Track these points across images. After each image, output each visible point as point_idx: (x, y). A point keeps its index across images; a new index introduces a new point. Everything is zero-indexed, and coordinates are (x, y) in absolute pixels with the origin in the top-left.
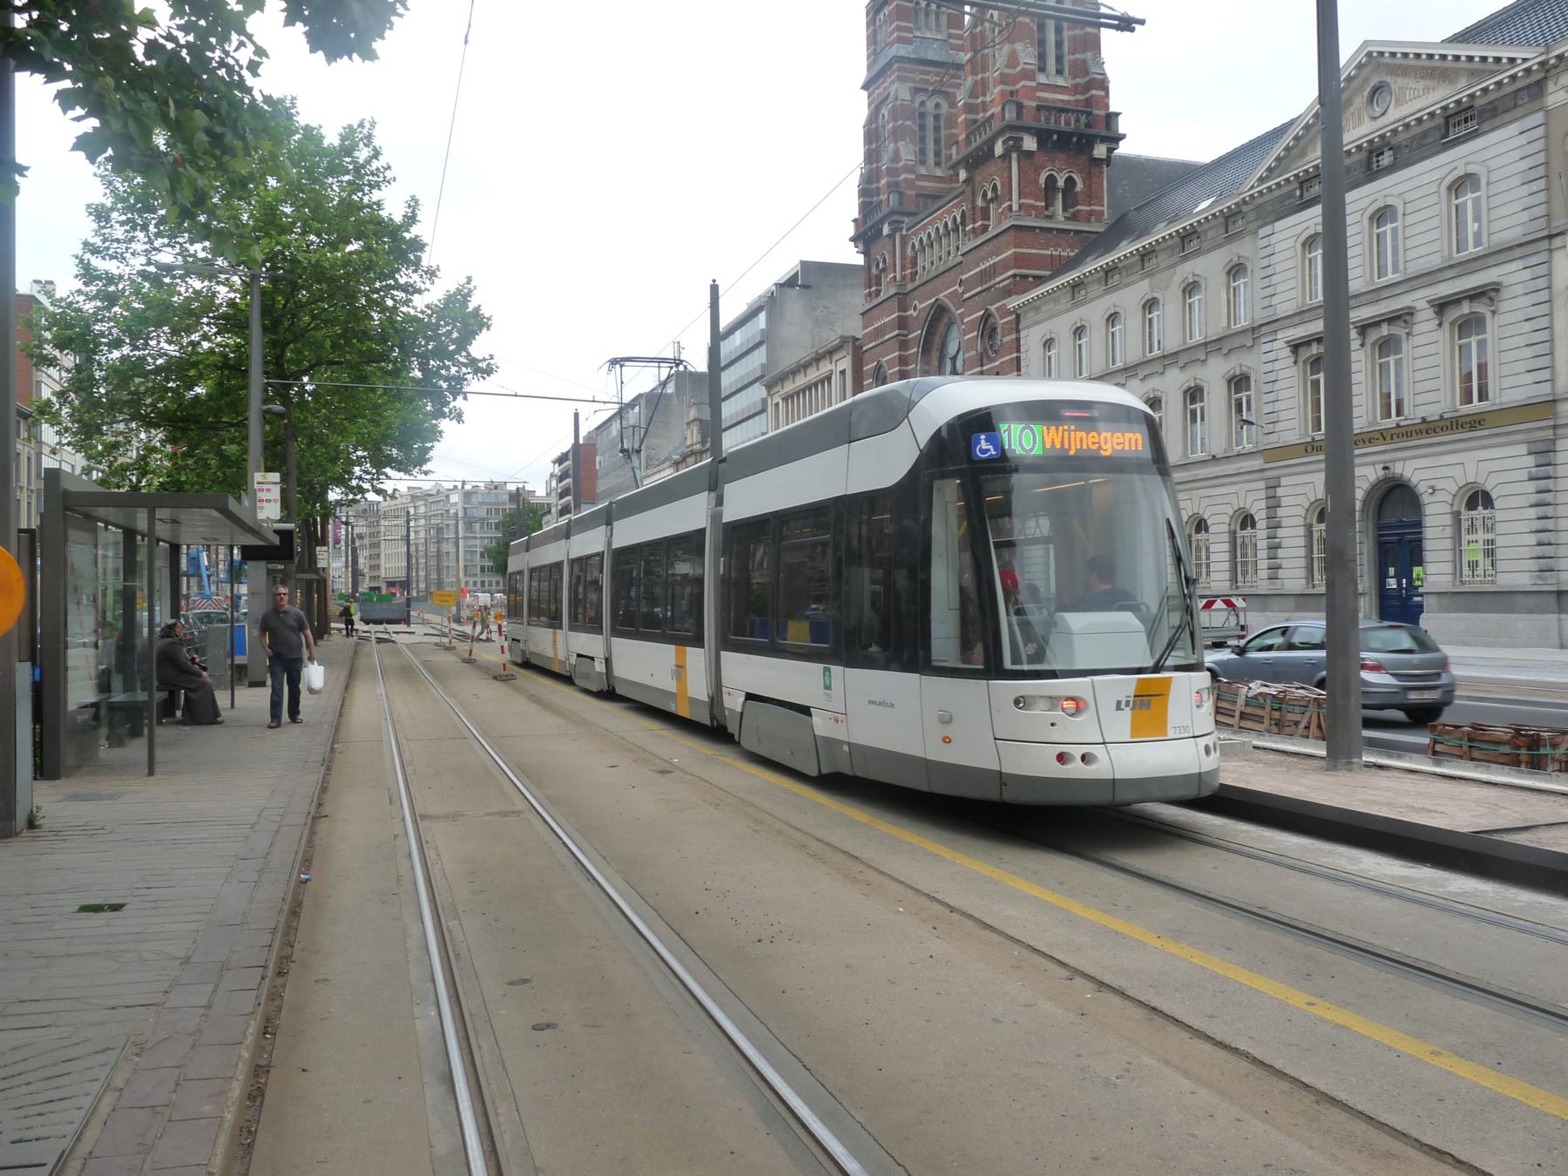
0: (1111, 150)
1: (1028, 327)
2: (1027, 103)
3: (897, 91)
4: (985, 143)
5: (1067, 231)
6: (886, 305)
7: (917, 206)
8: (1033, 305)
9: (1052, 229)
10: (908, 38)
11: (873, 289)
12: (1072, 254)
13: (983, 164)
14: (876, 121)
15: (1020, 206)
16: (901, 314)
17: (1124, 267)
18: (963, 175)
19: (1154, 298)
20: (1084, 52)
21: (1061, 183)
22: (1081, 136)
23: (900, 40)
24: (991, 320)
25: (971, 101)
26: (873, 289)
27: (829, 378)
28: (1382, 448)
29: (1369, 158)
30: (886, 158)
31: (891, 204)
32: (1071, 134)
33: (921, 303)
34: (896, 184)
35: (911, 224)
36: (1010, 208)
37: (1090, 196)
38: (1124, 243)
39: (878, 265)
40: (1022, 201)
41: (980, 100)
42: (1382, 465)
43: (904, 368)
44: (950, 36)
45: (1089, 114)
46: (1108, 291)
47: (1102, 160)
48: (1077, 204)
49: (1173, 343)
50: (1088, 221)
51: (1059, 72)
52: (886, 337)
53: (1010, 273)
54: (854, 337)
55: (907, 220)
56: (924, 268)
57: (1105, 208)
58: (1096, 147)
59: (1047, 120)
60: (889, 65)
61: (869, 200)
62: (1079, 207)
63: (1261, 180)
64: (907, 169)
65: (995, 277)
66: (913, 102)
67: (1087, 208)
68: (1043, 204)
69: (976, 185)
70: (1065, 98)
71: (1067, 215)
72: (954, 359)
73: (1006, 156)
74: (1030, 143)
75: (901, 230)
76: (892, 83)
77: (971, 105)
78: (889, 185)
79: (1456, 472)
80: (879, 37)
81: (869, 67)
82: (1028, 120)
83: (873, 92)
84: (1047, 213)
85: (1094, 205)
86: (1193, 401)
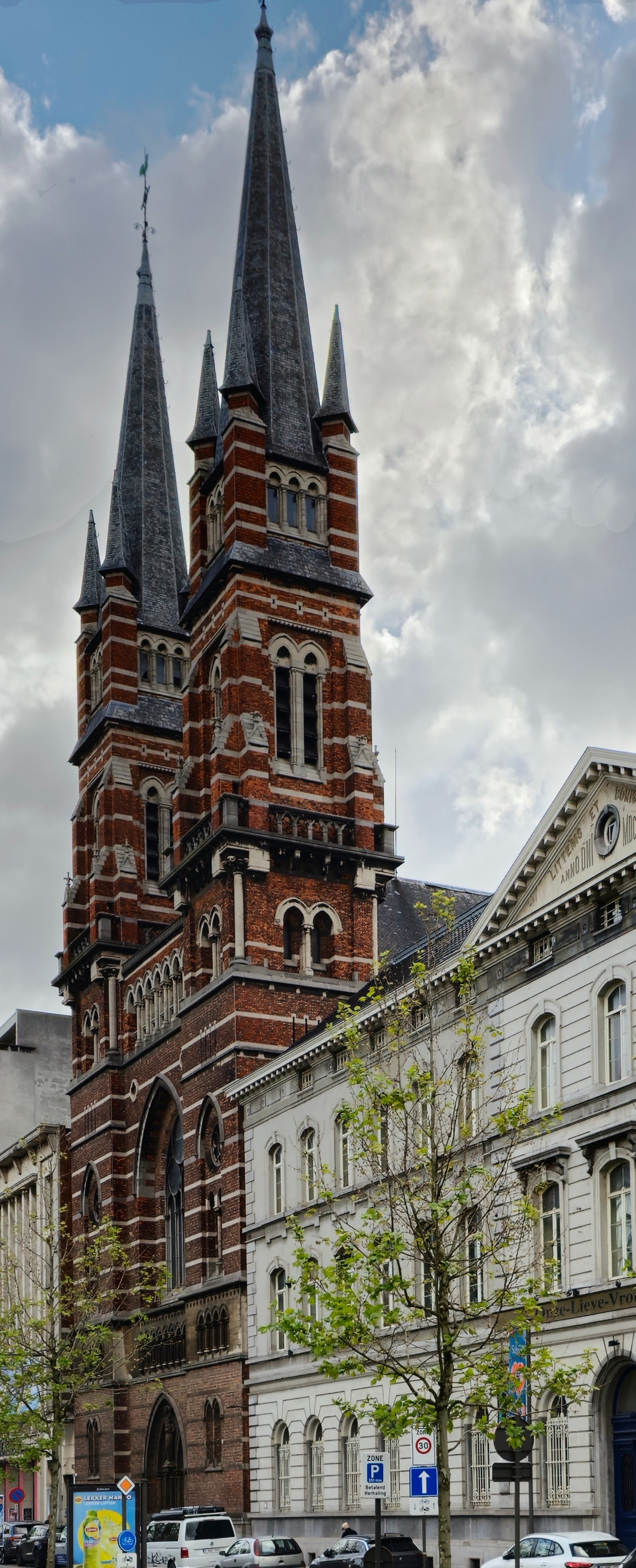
1: (252, 1126)
2: (254, 801)
3: (111, 770)
6: (96, 1082)
8: (254, 1091)
11: (84, 1058)
13: (203, 887)
15: (246, 949)
16: (116, 1097)
20: (345, 736)
21: (309, 921)
23: (117, 695)
25: (190, 793)
26: (84, 1058)
27: (32, 1186)
28: (608, 1316)
29: (599, 913)
30: (97, 864)
32: (325, 852)
35: (129, 965)
36: (232, 952)
37: (352, 943)
39: (88, 1024)
40: (249, 943)
41: (202, 793)
42: (608, 1340)
43: (121, 1177)
45: (351, 825)
47: (369, 892)
51: (311, 760)
52: (98, 1129)
53: (232, 1046)
54: (62, 1127)
55: (123, 959)
58: (359, 872)
59: (288, 830)
61: (78, 926)
62: (337, 958)
63: (488, 933)
64: (126, 885)
66: (136, 786)
67: (348, 960)
68: (281, 950)
70: (318, 798)
71: (318, 967)
73: (226, 877)
74: (259, 860)
76: (107, 757)
77: (189, 797)
78: (99, 906)
80: (93, 689)
84: (288, 963)
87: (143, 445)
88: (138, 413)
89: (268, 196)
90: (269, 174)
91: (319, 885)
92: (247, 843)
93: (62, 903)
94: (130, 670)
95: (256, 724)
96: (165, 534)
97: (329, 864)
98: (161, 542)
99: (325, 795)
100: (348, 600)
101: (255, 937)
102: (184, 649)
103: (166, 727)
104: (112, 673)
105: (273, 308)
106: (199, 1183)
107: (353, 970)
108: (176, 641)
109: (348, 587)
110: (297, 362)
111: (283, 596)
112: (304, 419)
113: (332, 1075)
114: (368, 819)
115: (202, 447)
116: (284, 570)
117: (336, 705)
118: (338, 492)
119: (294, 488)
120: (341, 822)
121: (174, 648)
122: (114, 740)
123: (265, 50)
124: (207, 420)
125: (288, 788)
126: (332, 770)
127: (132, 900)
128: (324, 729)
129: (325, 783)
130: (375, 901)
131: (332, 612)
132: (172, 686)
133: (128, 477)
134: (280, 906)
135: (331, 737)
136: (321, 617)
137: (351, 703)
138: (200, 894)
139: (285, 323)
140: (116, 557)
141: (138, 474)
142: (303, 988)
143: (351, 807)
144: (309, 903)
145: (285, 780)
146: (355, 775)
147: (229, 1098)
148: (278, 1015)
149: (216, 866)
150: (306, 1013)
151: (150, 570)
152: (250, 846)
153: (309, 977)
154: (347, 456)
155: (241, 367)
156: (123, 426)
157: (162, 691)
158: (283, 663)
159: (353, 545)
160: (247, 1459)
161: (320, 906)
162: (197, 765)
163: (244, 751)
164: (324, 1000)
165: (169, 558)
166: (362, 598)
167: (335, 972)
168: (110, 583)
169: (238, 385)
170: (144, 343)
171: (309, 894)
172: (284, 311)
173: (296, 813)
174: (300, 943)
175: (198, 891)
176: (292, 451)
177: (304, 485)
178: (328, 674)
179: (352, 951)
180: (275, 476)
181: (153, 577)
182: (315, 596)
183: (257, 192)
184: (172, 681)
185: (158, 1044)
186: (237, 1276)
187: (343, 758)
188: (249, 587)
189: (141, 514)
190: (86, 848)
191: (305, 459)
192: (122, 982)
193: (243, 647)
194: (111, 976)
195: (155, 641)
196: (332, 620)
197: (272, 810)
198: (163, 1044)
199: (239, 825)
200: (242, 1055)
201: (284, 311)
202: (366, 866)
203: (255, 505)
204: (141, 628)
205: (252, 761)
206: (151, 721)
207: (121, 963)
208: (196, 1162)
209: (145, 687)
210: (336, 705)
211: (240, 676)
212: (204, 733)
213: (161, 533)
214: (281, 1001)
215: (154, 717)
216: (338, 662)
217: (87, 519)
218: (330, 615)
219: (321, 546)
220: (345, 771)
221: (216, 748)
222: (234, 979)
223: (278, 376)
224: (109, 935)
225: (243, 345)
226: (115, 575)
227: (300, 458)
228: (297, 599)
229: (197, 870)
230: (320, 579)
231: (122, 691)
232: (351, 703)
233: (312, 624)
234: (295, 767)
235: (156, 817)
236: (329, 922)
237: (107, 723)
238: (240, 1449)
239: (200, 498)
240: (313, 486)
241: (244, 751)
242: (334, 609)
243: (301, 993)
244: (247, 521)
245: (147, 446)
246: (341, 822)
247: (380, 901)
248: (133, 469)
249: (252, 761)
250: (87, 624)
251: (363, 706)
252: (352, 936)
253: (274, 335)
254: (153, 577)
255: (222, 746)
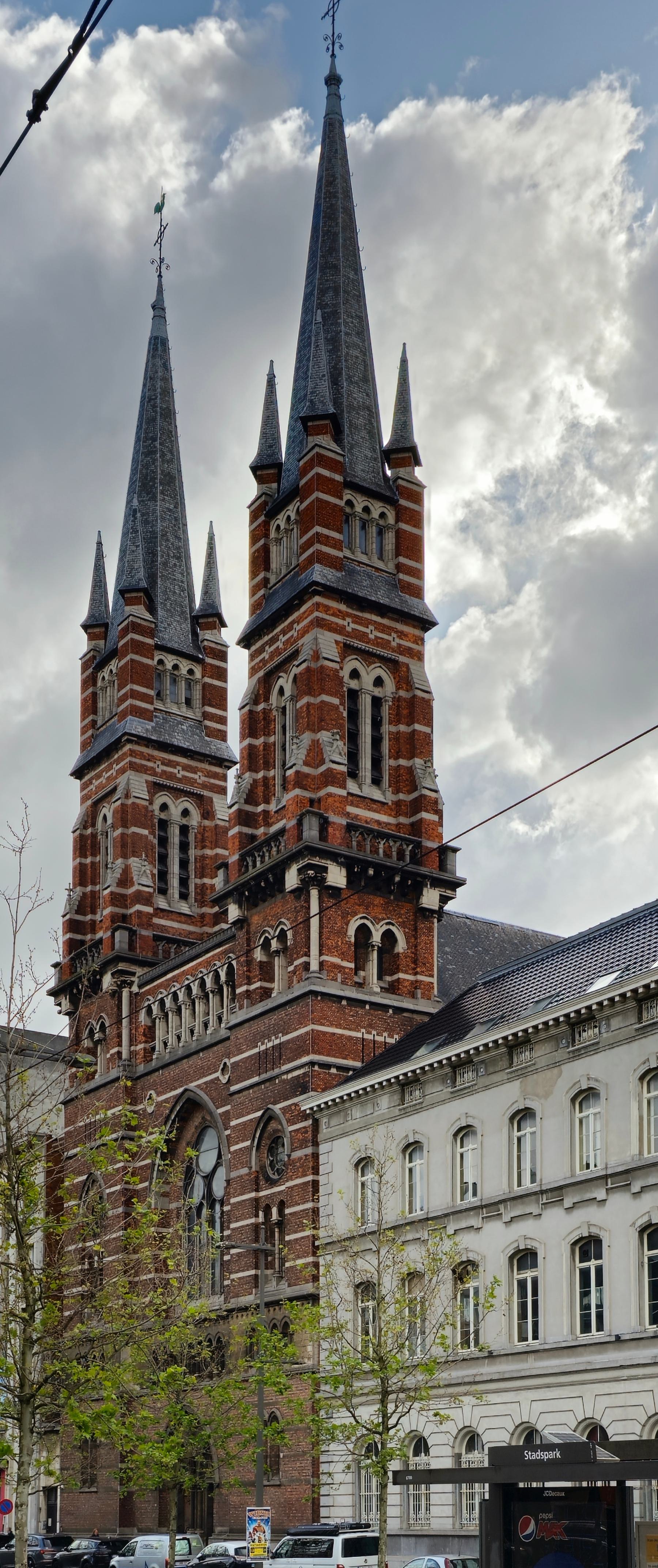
0: (444, 900)
1: (332, 1139)
2: (333, 818)
3: (128, 784)
4: (271, 869)
5: (385, 1007)
7: (155, 954)
9: (363, 1003)
10: (147, 710)
12: (392, 1041)
13: (264, 901)
14: (93, 825)
15: (321, 964)
17: (482, 1062)
18: (234, 912)
19: (527, 1109)
20: (411, 757)
21: (376, 938)
22: (405, 875)
24: (273, 1125)
31: (117, 946)
32: (393, 871)
33: (159, 1094)
34: (124, 918)
36: (306, 966)
37: (415, 962)
38: (422, 1051)
41: (260, 808)
44: (206, 716)
45: (418, 845)
46: (458, 1094)
47: (432, 911)
48: (397, 970)
49: (393, 1212)
50: (413, 996)
53: (305, 1059)
55: (139, 971)
56: (165, 1044)
57: (434, 980)
60: (115, 746)
61: (79, 937)
62: (401, 975)
65: (281, 1065)
66: (151, 803)
67: (411, 977)
68: (352, 965)
69: (253, 928)
70: (384, 818)
72: (209, 1178)
73: (301, 892)
74: (337, 876)
75: (131, 984)
76: (122, 771)
77: (247, 813)
78: (114, 918)
79: (576, 1404)
80: (100, 705)
81: (84, 745)
82: (336, 841)
83: (90, 782)
84: (356, 979)
85: (422, 973)
86: (585, 1257)
87: (159, 472)
88: (154, 439)
89: (340, 235)
90: (341, 215)
91: (386, 903)
92: (327, 859)
93: (62, 913)
94: (147, 687)
95: (335, 742)
96: (179, 558)
97: (399, 882)
98: (175, 565)
99: (390, 815)
100: (414, 627)
101: (330, 952)
102: (195, 670)
103: (180, 745)
104: (131, 690)
105: (346, 342)
106: (253, 1195)
107: (416, 988)
108: (189, 662)
109: (417, 614)
110: (367, 395)
111: (357, 620)
112: (374, 451)
113: (450, 1090)
114: (433, 841)
115: (265, 472)
116: (360, 594)
117: (402, 728)
118: (407, 523)
119: (365, 516)
120: (408, 842)
121: (187, 669)
122: (131, 755)
123: (334, 97)
124: (270, 447)
125: (357, 807)
126: (397, 791)
127: (148, 913)
128: (390, 751)
129: (390, 803)
130: (435, 920)
131: (400, 637)
132: (184, 705)
133: (143, 501)
134: (352, 922)
135: (396, 758)
136: (389, 642)
137: (417, 727)
138: (259, 908)
139: (357, 357)
140: (136, 577)
141: (154, 499)
142: (372, 1004)
143: (417, 828)
144: (377, 920)
145: (355, 798)
146: (423, 796)
147: (305, 1110)
148: (350, 1029)
149: (292, 879)
150: (373, 1028)
151: (165, 592)
152: (329, 862)
153: (377, 993)
154: (414, 488)
155: (322, 396)
156: (136, 452)
157: (174, 709)
158: (354, 684)
159: (419, 574)
160: (316, 1474)
161: (387, 924)
162: (255, 781)
163: (322, 768)
164: (390, 1016)
165: (182, 582)
166: (426, 624)
167: (398, 989)
168: (129, 602)
169: (320, 412)
170: (160, 374)
171: (377, 911)
172: (356, 346)
173: (370, 831)
174: (366, 960)
175: (256, 906)
176: (365, 480)
177: (375, 514)
178: (394, 697)
179: (414, 969)
180: (349, 503)
181: (168, 599)
182: (385, 621)
183: (329, 231)
184: (184, 701)
185: (187, 1056)
186: (308, 1288)
187: (407, 780)
188: (327, 609)
189: (156, 537)
190: (88, 860)
191: (378, 489)
192: (137, 994)
193: (322, 667)
194: (125, 987)
195: (170, 661)
196: (399, 645)
197: (350, 828)
198: (195, 1056)
199: (320, 839)
200: (316, 1068)
201: (356, 346)
202: (431, 886)
203: (333, 530)
204: (159, 647)
205: (330, 778)
206: (166, 738)
207: (137, 975)
208: (249, 1174)
209: (159, 705)
210: (402, 728)
211: (320, 695)
212: (264, 750)
213: (174, 556)
214: (353, 1016)
215: (169, 735)
216: (404, 686)
217: (95, 540)
218: (398, 641)
219: (390, 573)
220: (410, 792)
221: (294, 764)
222: (311, 992)
223: (351, 407)
224: (126, 946)
225: (324, 376)
226: (134, 595)
227: (373, 487)
228: (370, 623)
229: (263, 884)
230: (393, 605)
231: (140, 707)
232: (417, 727)
233: (382, 648)
234: (364, 787)
235: (166, 833)
236: (395, 940)
237: (126, 738)
238: (307, 1463)
239: (264, 521)
240: (383, 515)
241: (322, 768)
242: (402, 635)
243: (370, 1009)
244: (326, 545)
245: (162, 471)
246: (408, 842)
247: (439, 921)
248: (148, 494)
249: (330, 778)
250: (94, 642)
251: (426, 729)
252: (416, 954)
253: (347, 367)
254: (168, 599)
255: (301, 762)
